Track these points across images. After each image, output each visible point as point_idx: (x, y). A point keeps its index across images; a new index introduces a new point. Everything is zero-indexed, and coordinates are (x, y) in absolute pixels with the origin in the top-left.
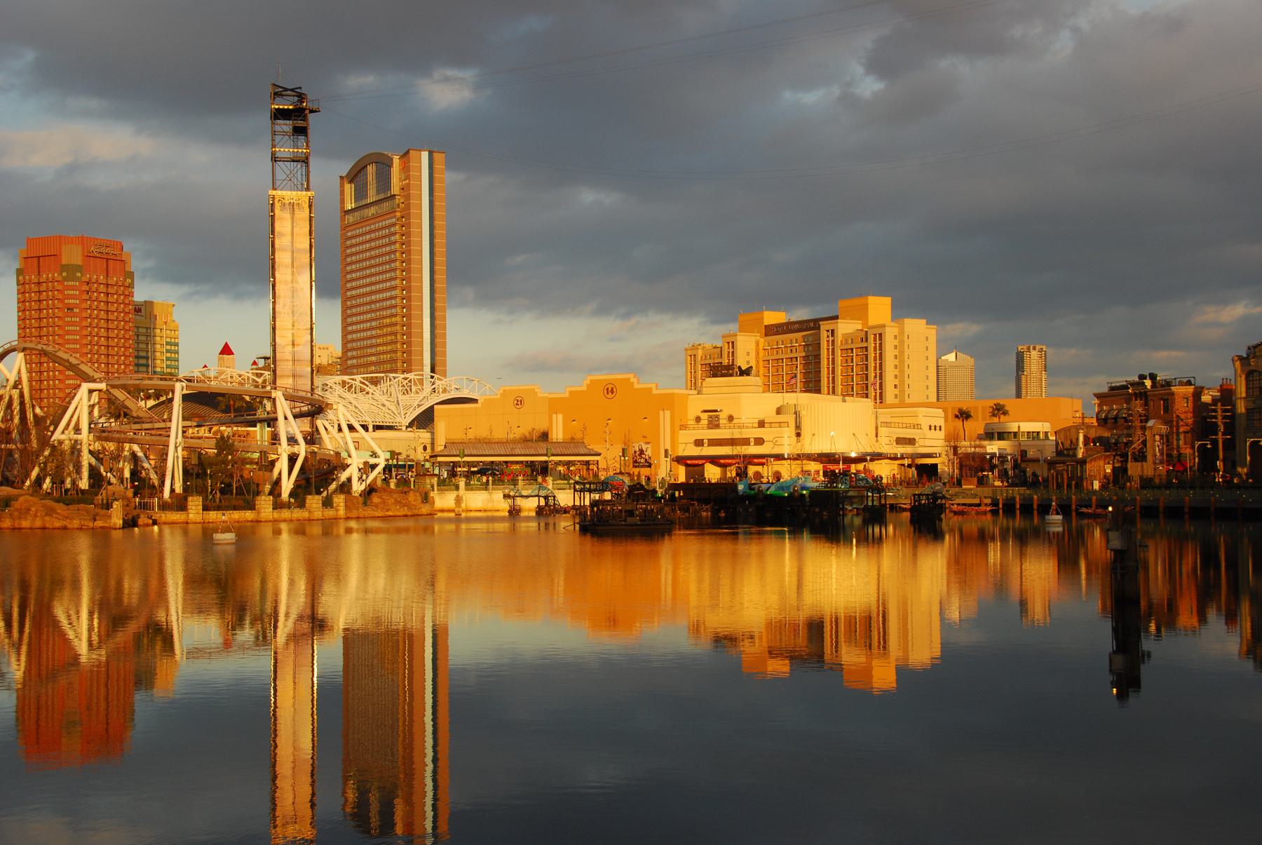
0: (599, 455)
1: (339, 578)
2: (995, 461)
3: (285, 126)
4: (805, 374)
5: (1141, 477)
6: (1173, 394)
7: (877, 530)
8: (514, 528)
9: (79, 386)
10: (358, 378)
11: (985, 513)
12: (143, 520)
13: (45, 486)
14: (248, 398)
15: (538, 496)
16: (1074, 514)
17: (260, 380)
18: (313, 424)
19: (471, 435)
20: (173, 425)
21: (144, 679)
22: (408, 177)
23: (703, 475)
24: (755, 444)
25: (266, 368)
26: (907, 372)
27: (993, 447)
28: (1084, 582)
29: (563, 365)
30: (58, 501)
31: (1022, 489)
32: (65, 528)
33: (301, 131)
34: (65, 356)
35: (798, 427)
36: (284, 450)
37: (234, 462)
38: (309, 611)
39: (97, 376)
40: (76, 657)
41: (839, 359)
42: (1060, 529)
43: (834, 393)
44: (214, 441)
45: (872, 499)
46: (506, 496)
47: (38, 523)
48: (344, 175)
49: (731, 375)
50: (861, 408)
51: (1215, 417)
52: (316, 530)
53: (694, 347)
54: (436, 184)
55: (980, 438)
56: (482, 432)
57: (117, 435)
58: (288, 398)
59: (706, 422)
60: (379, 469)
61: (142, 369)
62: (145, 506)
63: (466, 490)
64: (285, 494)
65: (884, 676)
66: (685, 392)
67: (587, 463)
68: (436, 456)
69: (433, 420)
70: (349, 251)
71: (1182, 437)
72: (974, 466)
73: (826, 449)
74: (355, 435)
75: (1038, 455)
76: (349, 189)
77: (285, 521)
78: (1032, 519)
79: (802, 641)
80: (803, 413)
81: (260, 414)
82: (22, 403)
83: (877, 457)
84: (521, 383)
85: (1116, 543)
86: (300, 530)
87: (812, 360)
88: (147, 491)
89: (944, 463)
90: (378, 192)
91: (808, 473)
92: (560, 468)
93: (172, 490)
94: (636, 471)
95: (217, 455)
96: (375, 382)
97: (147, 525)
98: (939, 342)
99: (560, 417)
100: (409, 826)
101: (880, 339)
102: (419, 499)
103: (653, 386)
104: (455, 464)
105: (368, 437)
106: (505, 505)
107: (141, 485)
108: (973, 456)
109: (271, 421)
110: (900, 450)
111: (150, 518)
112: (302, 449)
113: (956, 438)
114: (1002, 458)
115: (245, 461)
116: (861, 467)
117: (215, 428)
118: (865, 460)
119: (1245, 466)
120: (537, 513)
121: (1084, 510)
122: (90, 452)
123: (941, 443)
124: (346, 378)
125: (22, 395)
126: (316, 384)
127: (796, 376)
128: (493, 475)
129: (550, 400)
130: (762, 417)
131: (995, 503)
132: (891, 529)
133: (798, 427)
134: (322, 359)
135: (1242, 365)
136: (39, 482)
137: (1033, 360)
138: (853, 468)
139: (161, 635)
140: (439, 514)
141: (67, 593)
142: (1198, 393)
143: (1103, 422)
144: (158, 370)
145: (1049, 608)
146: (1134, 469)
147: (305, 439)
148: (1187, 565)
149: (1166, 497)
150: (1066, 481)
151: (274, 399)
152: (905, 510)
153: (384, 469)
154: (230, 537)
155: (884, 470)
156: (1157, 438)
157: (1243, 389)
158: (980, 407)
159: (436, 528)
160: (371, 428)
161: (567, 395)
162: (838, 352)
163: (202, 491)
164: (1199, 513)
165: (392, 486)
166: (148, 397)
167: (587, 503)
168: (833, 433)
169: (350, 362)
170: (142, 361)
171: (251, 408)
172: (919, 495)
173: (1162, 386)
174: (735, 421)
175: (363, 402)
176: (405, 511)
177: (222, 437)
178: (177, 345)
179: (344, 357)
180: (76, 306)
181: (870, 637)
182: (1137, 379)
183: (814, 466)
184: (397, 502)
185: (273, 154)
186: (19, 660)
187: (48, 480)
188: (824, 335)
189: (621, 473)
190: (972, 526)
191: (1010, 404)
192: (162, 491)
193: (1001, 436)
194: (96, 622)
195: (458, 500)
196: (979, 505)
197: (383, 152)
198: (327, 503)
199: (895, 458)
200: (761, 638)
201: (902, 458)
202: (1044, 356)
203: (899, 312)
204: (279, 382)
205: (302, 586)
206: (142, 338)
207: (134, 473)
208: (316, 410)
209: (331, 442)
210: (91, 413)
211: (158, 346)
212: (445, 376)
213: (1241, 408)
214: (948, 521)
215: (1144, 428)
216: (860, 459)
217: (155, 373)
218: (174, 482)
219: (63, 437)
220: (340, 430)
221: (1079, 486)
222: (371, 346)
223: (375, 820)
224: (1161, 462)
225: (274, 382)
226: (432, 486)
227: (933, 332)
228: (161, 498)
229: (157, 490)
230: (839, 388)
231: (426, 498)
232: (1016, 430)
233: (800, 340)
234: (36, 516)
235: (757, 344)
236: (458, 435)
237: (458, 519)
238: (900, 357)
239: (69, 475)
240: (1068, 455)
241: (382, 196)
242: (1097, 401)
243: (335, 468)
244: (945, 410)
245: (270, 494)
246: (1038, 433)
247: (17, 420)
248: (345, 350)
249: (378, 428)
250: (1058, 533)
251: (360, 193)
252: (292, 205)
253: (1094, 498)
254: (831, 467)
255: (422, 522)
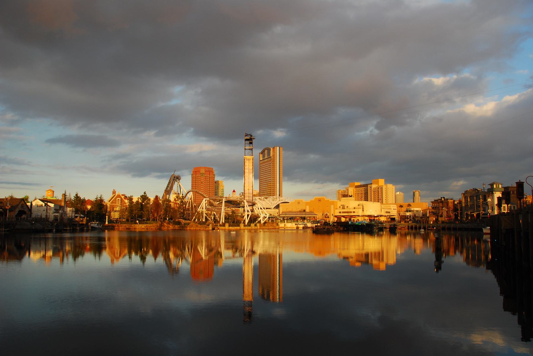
0: (317, 215)
1: (258, 243)
2: (409, 217)
3: (248, 142)
4: (365, 197)
5: (442, 221)
6: (448, 202)
7: (381, 233)
8: (297, 232)
9: (203, 199)
10: (263, 197)
11: (406, 229)
12: (216, 228)
13: (196, 221)
14: (238, 202)
15: (303, 224)
16: (426, 229)
17: (241, 198)
18: (252, 208)
19: (288, 210)
20: (223, 208)
21: (216, 263)
22: (274, 153)
23: (341, 220)
24: (353, 213)
25: (242, 195)
26: (388, 196)
27: (408, 214)
28: (429, 245)
29: (307, 195)
30: (198, 224)
31: (415, 224)
32: (200, 230)
33: (251, 143)
34: (201, 193)
35: (363, 209)
36: (246, 213)
37: (235, 216)
38: (251, 249)
39: (207, 197)
40: (202, 259)
41: (372, 194)
42: (423, 233)
43: (371, 201)
44: (231, 211)
45: (380, 226)
46: (296, 224)
47: (195, 229)
48: (260, 152)
49: (347, 197)
50: (377, 205)
51: (458, 207)
52: (253, 231)
53: (339, 191)
54: (280, 154)
55: (405, 212)
56: (290, 210)
57: (211, 210)
58: (247, 202)
59: (342, 208)
60: (267, 218)
61: (216, 195)
62: (216, 226)
63: (287, 223)
64: (246, 223)
65: (382, 266)
66: (337, 201)
67: (314, 217)
68: (280, 215)
69: (279, 207)
70: (261, 169)
71: (451, 212)
72: (403, 218)
73: (369, 214)
74: (262, 210)
75: (418, 216)
76: (261, 155)
77: (246, 229)
78: (417, 231)
79: (363, 259)
80: (364, 206)
81: (241, 205)
82: (192, 203)
83: (381, 216)
84: (299, 199)
85: (436, 236)
86: (250, 231)
87: (366, 194)
88: (217, 222)
89: (396, 217)
90: (268, 156)
91: (365, 220)
92: (308, 218)
93: (222, 222)
94: (326, 219)
95: (232, 214)
96: (266, 198)
97: (217, 229)
98: (395, 189)
99: (308, 206)
100: (273, 299)
101: (382, 189)
102: (276, 225)
103: (330, 199)
104: (284, 217)
105: (265, 211)
106: (295, 226)
107: (216, 221)
108: (403, 216)
109: (244, 207)
110: (387, 214)
111: (217, 228)
112: (250, 213)
113: (400, 212)
114: (410, 216)
115: (238, 216)
116: (377, 218)
117: (231, 208)
118: (379, 217)
119: (465, 218)
120: (303, 228)
121: (429, 228)
122: (205, 213)
123: (396, 213)
124: (260, 197)
125: (192, 201)
126: (253, 199)
127: (362, 197)
128: (293, 219)
129: (306, 202)
130: (354, 207)
131: (408, 227)
132: (384, 232)
133: (363, 209)
134: (255, 193)
135: (463, 195)
136: (195, 220)
137: (417, 194)
138: (376, 219)
139: (220, 254)
140: (280, 228)
141: (200, 244)
142: (454, 202)
143: (433, 208)
144: (220, 195)
145: (421, 251)
146: (440, 219)
147: (251, 211)
148: (452, 240)
149: (447, 225)
150: (425, 221)
151: (244, 202)
152: (388, 228)
153: (268, 218)
154: (234, 232)
155: (383, 219)
156: (445, 212)
157: (464, 201)
158: (405, 204)
159: (280, 231)
160: (265, 209)
161: (310, 201)
162: (372, 192)
163: (228, 222)
164: (455, 229)
165: (270, 222)
166: (217, 202)
167: (314, 226)
168: (371, 210)
169: (261, 194)
170: (216, 194)
171: (239, 204)
172: (391, 225)
173: (446, 200)
174: (348, 208)
175: (264, 203)
176: (273, 227)
177: (233, 210)
178: (224, 190)
179: (260, 193)
180: (203, 182)
181: (380, 256)
182: (440, 198)
183: (366, 218)
184: (271, 225)
185: (245, 148)
186: (191, 257)
187: (197, 219)
188: (369, 188)
189: (322, 219)
190: (403, 232)
191: (412, 204)
192: (220, 222)
193: (410, 211)
194: (206, 250)
195: (285, 225)
196: (405, 227)
197: (269, 147)
198: (256, 225)
199: (385, 216)
200: (354, 257)
201: (387, 216)
202: (419, 193)
203: (386, 182)
204: (245, 198)
205: (250, 243)
206: (216, 189)
207: (214, 218)
208: (253, 204)
209: (256, 212)
210: (205, 205)
211: (220, 190)
212: (282, 197)
213: (463, 205)
214: (398, 231)
215: (442, 210)
216: (377, 216)
217: (219, 196)
218: (222, 220)
219: (200, 210)
220: (258, 209)
221: (428, 223)
222: (266, 190)
223: (265, 296)
224: (446, 217)
225: (244, 198)
226: (279, 222)
227: (394, 187)
228: (220, 224)
229: (219, 222)
230: (372, 200)
231: (277, 224)
232: (413, 210)
233: (363, 189)
234: (194, 227)
235: (354, 190)
236: (285, 210)
237: (285, 230)
238: (386, 193)
239: (201, 218)
240: (425, 216)
241: (268, 157)
242: (431, 203)
243: (257, 217)
244: (397, 205)
245: (243, 223)
246: (418, 210)
247: (191, 206)
248: (260, 191)
249: (267, 209)
250: (423, 234)
251: (264, 156)
252: (249, 159)
253: (431, 226)
254: (371, 218)
255: (277, 230)
